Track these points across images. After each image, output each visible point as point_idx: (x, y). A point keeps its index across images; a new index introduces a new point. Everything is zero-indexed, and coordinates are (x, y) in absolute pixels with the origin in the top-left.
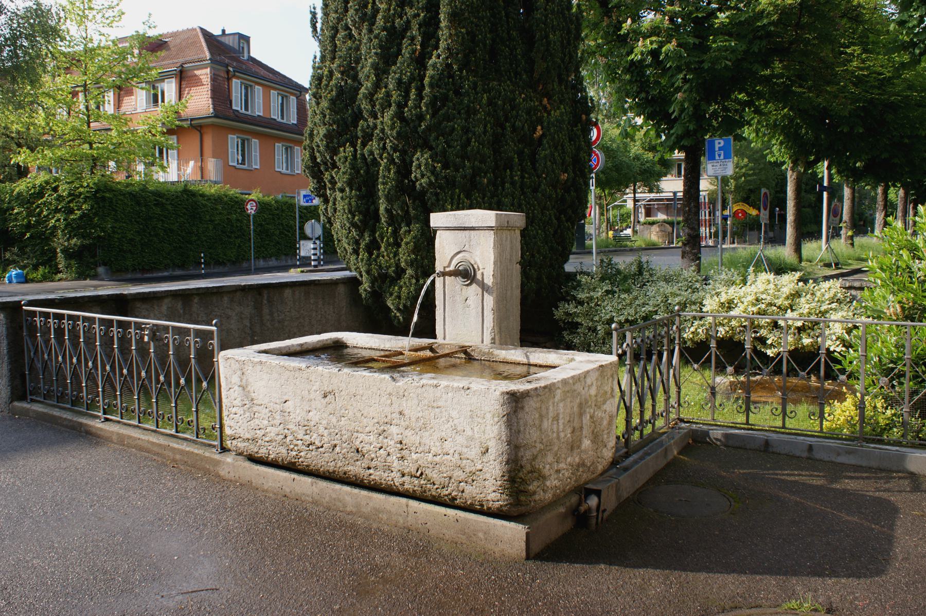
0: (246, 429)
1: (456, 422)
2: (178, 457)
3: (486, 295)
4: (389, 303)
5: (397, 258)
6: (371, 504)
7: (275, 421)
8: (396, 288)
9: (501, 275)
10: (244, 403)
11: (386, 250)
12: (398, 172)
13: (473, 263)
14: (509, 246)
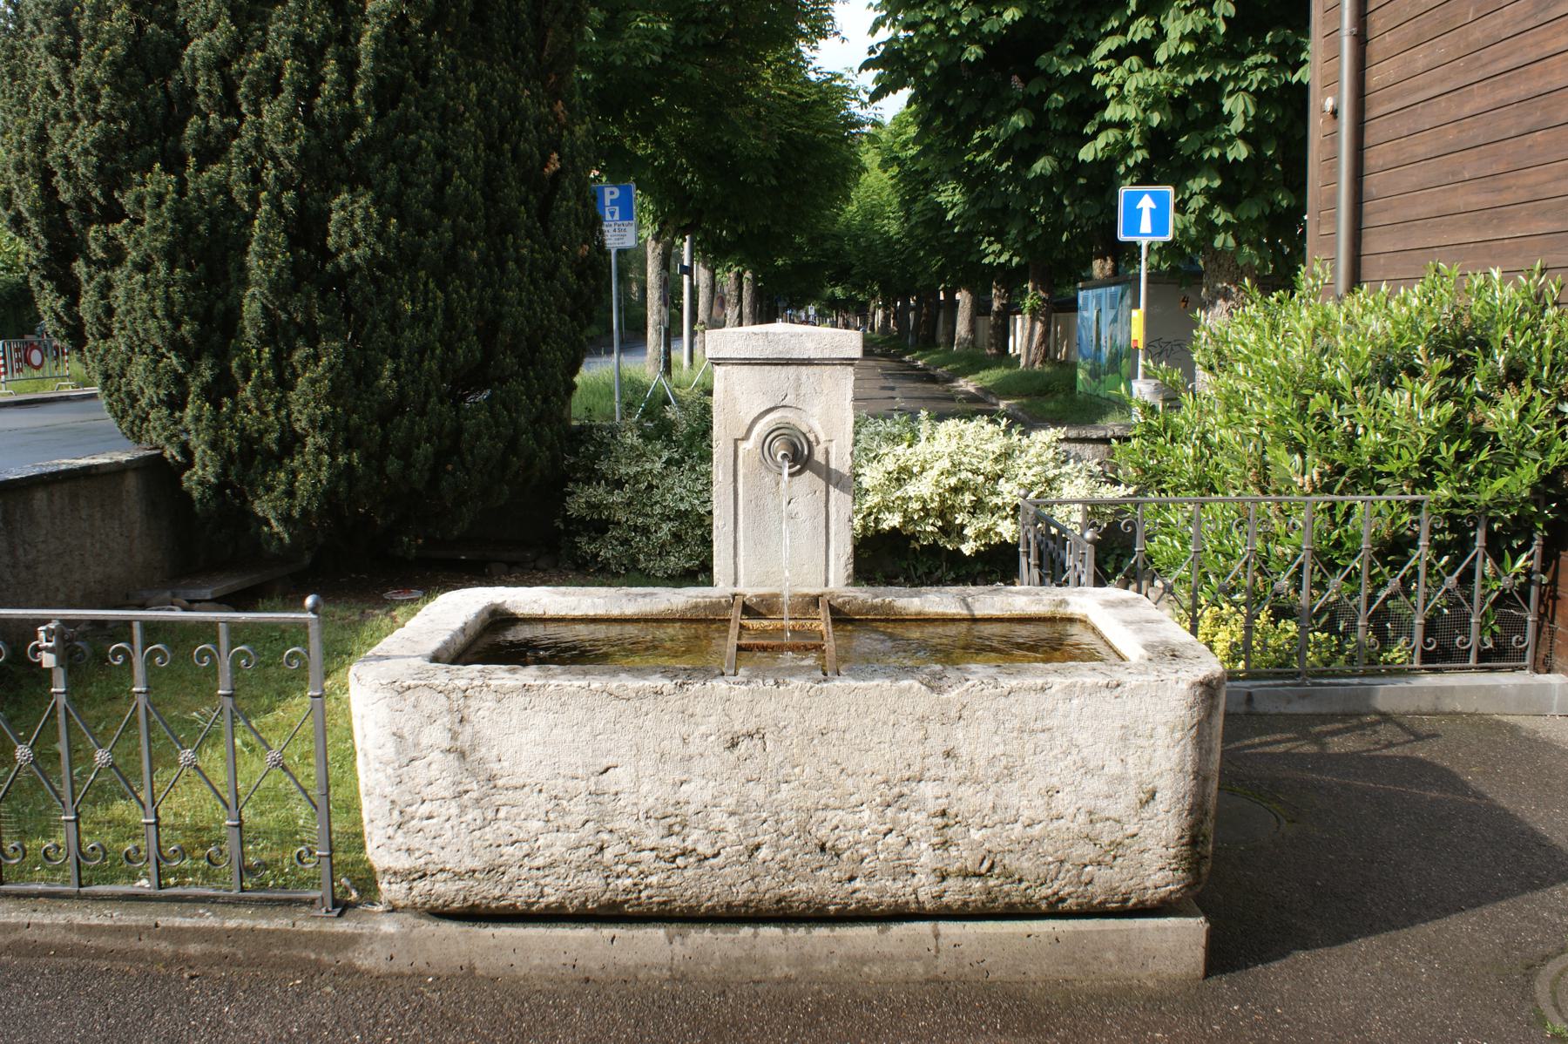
0: (465, 850)
1: (1085, 752)
2: (194, 949)
3: (831, 488)
5: (284, 413)
6: (841, 951)
7: (568, 820)
10: (461, 788)
13: (804, 429)
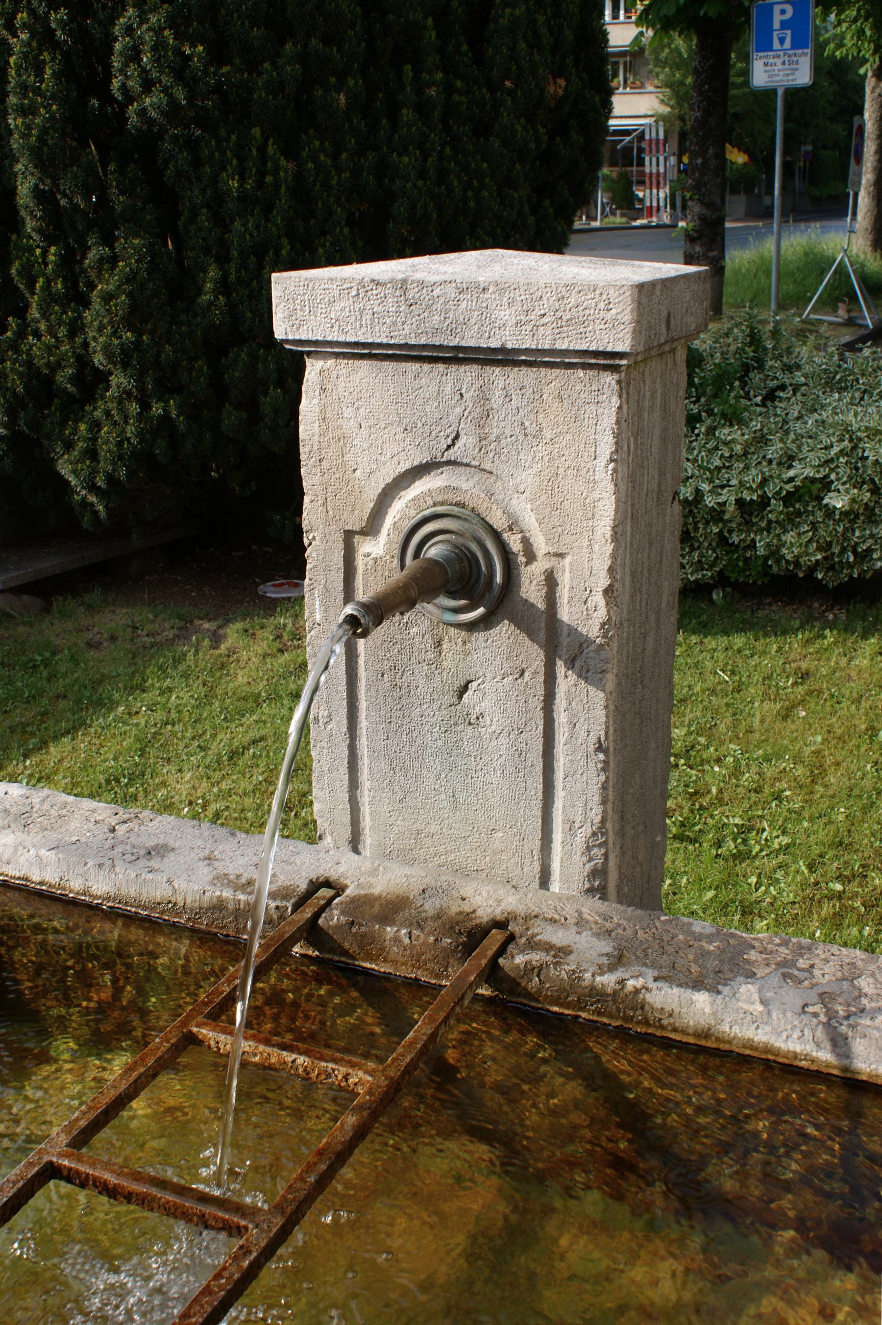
3: (560, 668)
4: (64, 469)
5: (79, 340)
8: (83, 427)
9: (633, 575)
11: (45, 316)
12: (65, 74)
13: (498, 521)
14: (657, 432)
